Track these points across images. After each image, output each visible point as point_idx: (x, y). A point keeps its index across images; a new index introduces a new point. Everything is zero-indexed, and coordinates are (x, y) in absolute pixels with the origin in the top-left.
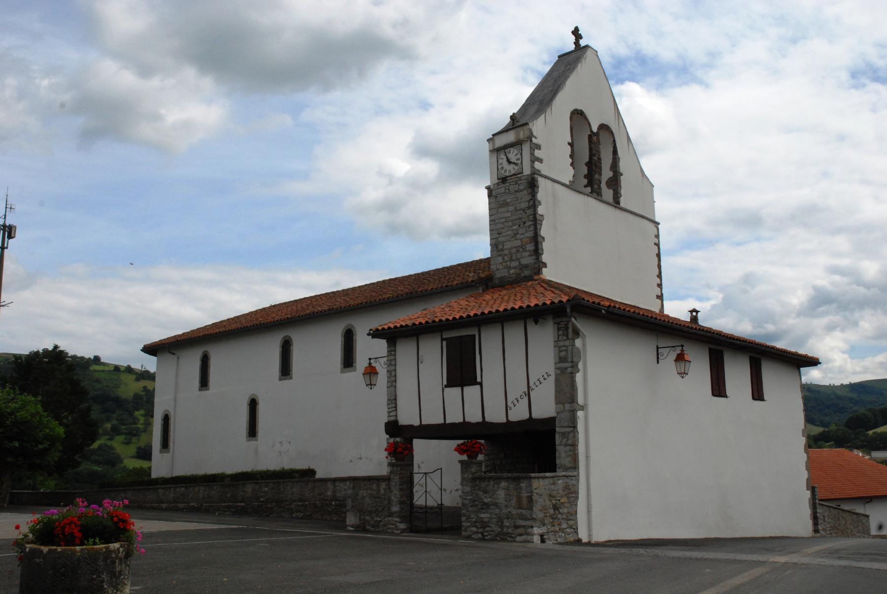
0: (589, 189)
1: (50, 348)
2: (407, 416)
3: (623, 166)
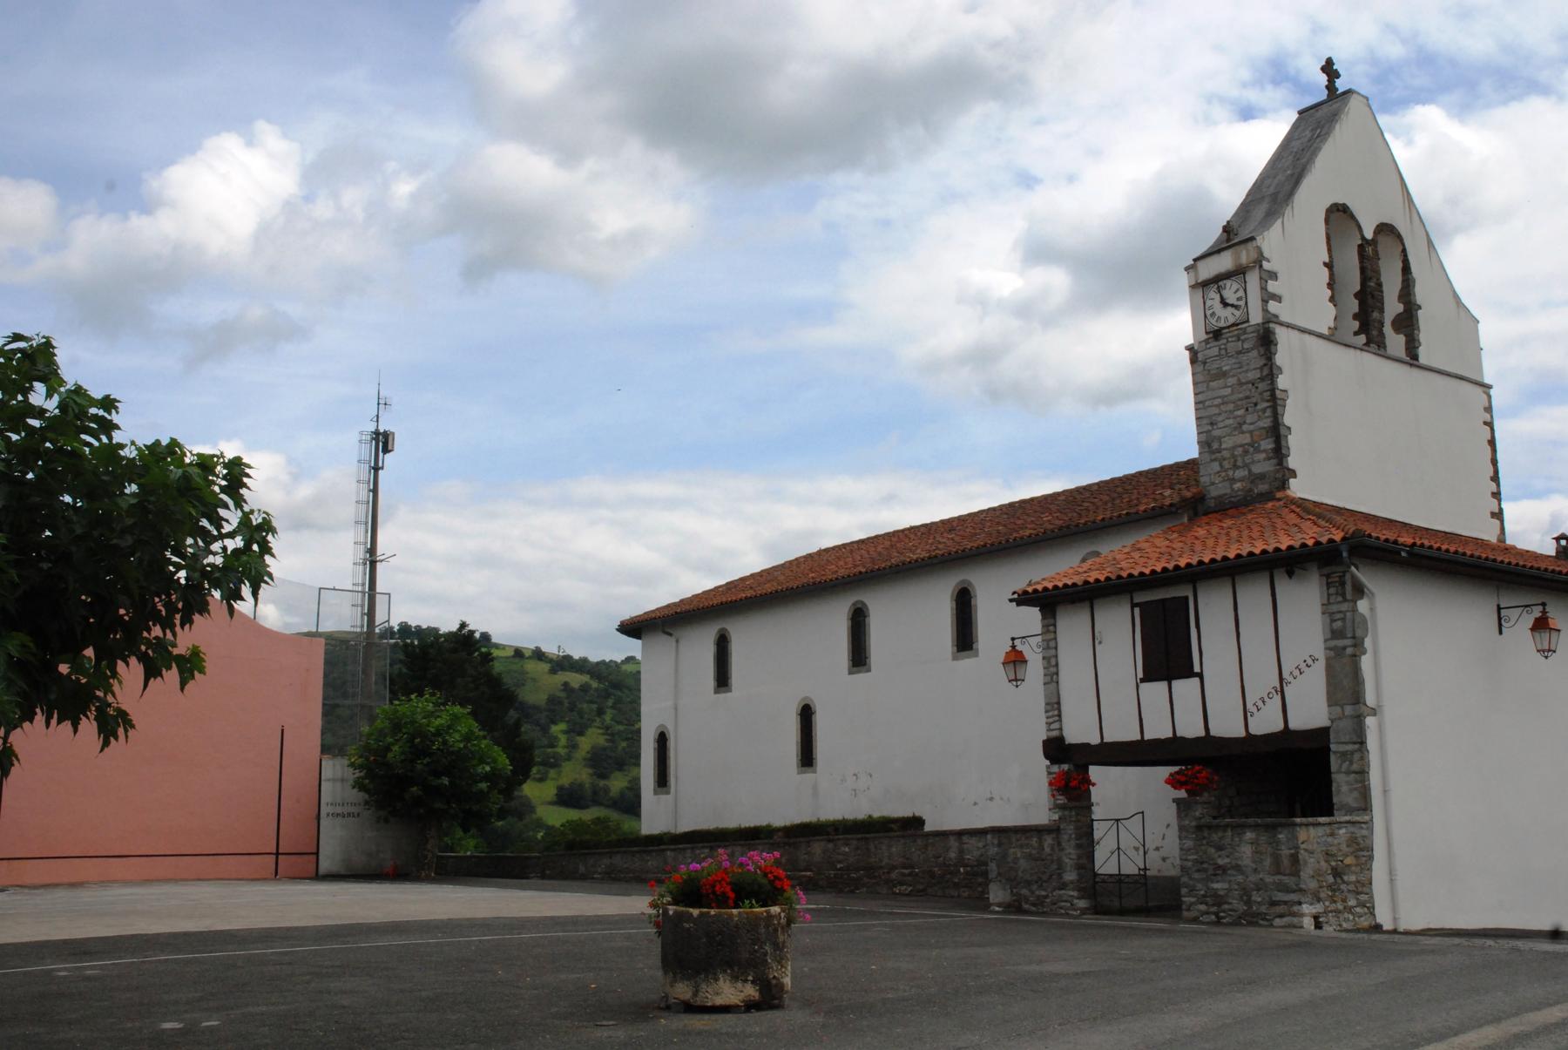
0: (1362, 339)
1: (454, 627)
2: (1080, 730)
3: (1421, 293)
